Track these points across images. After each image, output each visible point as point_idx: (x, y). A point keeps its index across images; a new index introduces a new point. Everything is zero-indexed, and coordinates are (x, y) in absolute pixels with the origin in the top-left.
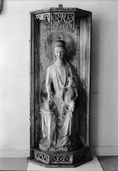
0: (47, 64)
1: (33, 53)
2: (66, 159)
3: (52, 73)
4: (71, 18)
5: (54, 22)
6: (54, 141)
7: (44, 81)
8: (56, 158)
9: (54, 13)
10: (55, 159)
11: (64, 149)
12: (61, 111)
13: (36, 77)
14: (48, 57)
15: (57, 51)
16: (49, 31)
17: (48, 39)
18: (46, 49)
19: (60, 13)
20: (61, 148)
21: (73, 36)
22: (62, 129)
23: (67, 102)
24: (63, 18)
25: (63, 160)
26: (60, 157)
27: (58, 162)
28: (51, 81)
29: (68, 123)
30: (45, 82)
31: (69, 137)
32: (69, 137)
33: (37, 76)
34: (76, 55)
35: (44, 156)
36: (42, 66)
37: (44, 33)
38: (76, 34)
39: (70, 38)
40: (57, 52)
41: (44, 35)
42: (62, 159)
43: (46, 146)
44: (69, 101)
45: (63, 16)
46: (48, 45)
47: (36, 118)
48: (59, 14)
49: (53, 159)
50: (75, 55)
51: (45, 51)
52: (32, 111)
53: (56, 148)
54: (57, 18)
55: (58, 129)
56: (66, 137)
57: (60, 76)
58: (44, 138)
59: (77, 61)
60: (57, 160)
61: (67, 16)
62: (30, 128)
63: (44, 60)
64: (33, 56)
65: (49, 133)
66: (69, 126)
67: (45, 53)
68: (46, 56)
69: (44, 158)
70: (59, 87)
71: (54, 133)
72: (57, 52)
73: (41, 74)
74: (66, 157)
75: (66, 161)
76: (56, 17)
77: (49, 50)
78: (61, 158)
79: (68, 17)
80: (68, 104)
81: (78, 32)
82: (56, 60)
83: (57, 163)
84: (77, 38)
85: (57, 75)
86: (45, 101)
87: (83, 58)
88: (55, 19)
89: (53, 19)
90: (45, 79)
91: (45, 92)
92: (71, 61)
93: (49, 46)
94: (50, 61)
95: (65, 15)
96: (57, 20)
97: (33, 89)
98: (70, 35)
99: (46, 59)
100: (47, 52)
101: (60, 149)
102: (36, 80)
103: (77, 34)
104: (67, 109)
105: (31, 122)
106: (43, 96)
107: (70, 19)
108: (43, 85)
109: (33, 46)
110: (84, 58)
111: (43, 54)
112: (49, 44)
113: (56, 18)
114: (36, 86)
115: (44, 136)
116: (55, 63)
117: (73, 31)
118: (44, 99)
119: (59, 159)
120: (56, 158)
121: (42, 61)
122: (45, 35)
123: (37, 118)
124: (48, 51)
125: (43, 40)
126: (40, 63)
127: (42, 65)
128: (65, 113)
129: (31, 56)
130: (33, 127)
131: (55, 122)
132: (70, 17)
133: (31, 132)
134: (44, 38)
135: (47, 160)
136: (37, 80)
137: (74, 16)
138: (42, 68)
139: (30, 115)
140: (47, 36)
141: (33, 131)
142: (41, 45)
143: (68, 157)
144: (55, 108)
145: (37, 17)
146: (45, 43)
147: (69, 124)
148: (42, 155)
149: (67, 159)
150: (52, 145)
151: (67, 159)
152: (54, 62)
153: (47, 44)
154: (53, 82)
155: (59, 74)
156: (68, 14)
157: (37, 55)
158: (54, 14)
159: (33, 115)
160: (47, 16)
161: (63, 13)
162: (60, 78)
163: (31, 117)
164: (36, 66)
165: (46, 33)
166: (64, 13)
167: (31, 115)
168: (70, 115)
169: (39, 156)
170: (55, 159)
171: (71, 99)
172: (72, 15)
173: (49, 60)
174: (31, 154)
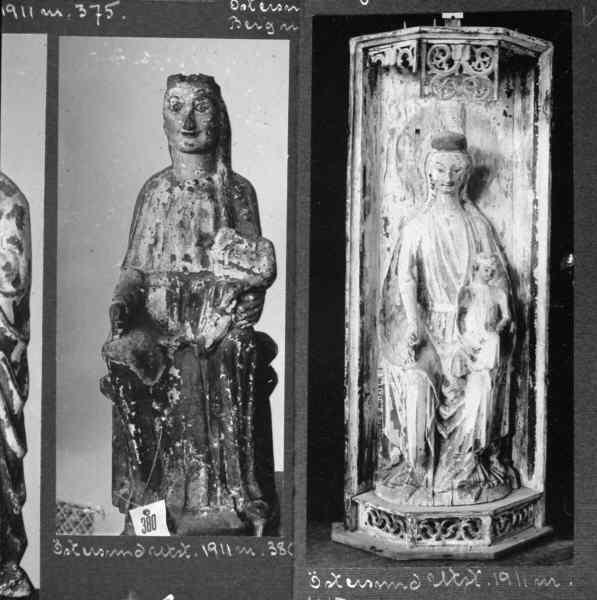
4: (486, 59)
12: (449, 370)
15: (442, 168)
18: (400, 161)
42: (456, 530)
50: (499, 182)
78: (450, 529)
89: (429, 63)
96: (441, 64)
107: (485, 63)
147: (479, 411)
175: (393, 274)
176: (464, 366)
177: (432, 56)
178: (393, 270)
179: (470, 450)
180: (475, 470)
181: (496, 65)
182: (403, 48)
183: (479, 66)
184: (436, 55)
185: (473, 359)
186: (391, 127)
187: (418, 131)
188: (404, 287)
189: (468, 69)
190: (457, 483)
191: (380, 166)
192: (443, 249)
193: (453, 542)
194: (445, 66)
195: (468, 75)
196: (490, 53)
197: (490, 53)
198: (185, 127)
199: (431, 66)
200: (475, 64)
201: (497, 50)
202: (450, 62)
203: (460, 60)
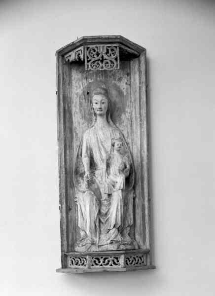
0: (84, 129)
1: (62, 110)
2: (113, 261)
3: (91, 138)
4: (113, 52)
5: (89, 59)
6: (96, 237)
7: (79, 153)
8: (98, 259)
9: (89, 46)
10: (97, 262)
11: (112, 247)
12: (104, 191)
13: (68, 147)
14: (85, 119)
15: (96, 102)
16: (85, 81)
17: (84, 92)
18: (82, 107)
19: (98, 46)
20: (106, 246)
21: (121, 87)
22: (108, 219)
23: (114, 176)
24: (102, 53)
25: (110, 263)
26: (105, 259)
27: (101, 265)
28: (90, 153)
29: (116, 207)
30: (81, 155)
31: (118, 228)
32: (118, 228)
33: (69, 146)
34: (127, 114)
35: (76, 260)
36: (75, 132)
37: (79, 84)
38: (125, 83)
39: (116, 90)
40: (96, 103)
41: (78, 86)
42: (109, 261)
43: (85, 245)
44: (116, 175)
45: (101, 50)
46: (84, 100)
47: (68, 209)
48: (97, 47)
49: (95, 262)
50: (125, 114)
51: (81, 111)
52: (62, 196)
53: (99, 246)
54: (94, 53)
55: (101, 219)
56: (114, 229)
57: (102, 142)
58: (82, 237)
59: (129, 122)
60: (101, 263)
61: (108, 50)
62: (61, 222)
63: (79, 123)
64: (62, 114)
65: (88, 224)
66: (117, 211)
67: (80, 112)
68: (82, 117)
69: (81, 262)
70: (101, 158)
71: (95, 225)
72: (96, 103)
73: (75, 144)
74: (114, 258)
75: (115, 263)
76: (92, 52)
77: (85, 108)
78: (106, 260)
79: (110, 51)
80: (115, 180)
81: (128, 81)
82: (96, 119)
83: (101, 267)
84: (127, 89)
85: (98, 141)
86: (82, 183)
87: (136, 117)
88: (91, 54)
89: (88, 55)
90: (80, 150)
91: (82, 171)
92: (120, 124)
93: (85, 102)
94: (88, 124)
95: (105, 48)
96: (94, 55)
97: (63, 163)
98: (115, 84)
99: (82, 121)
100: (83, 111)
101: (105, 247)
102: (68, 152)
103: (126, 84)
104: (114, 186)
105: (61, 212)
106: (78, 177)
107: (113, 54)
108: (79, 160)
109: (146, 225)
110: (138, 116)
111: (77, 114)
112: (85, 100)
113: (92, 53)
114: (68, 161)
115: (82, 233)
116: (95, 125)
117: (120, 79)
118: (81, 181)
119: (104, 262)
120: (98, 259)
121: (75, 125)
122: (80, 87)
123: (70, 209)
124: (84, 109)
125: (77, 94)
126: (74, 128)
127: (76, 130)
128: (110, 193)
129: (59, 115)
130: (65, 221)
131: (96, 207)
132: (112, 50)
133: (61, 228)
134: (78, 91)
135: (85, 263)
136: (69, 152)
137: (118, 50)
138: (77, 134)
139: (60, 203)
140: (82, 88)
141: (64, 227)
142: (74, 101)
143: (117, 258)
144: (96, 187)
145: (94, 104)
146: (80, 98)
147: (117, 208)
148: (79, 260)
149: (116, 261)
150: (93, 243)
151: (116, 261)
152: (93, 123)
153: (82, 100)
154: (92, 153)
155: (100, 140)
156: (109, 47)
157: (67, 115)
158: (89, 48)
159: (65, 203)
160: (80, 52)
161: (102, 45)
162: (102, 145)
163: (62, 205)
164: (68, 130)
165: (80, 83)
166: (103, 45)
167: (61, 202)
168: (118, 195)
169: (74, 263)
170: (97, 262)
171: (119, 172)
172: (116, 47)
173: (87, 123)
174: (63, 261)
175: (79, 156)
176: (110, 189)
177: (90, 52)
178: (79, 153)
179: (139, 242)
180: (116, 236)
181: (118, 55)
182: (77, 51)
183: (110, 55)
184: (91, 52)
185: (114, 186)
186: (76, 92)
187: (88, 93)
188: (85, 161)
189: (105, 57)
190: (109, 241)
191: (72, 109)
192: (100, 143)
193: (108, 266)
194: (95, 56)
195: (106, 59)
196: (115, 49)
197: (115, 49)
198: (87, 188)
199: (89, 57)
200: (109, 54)
201: (118, 48)
202: (98, 54)
203: (102, 53)
